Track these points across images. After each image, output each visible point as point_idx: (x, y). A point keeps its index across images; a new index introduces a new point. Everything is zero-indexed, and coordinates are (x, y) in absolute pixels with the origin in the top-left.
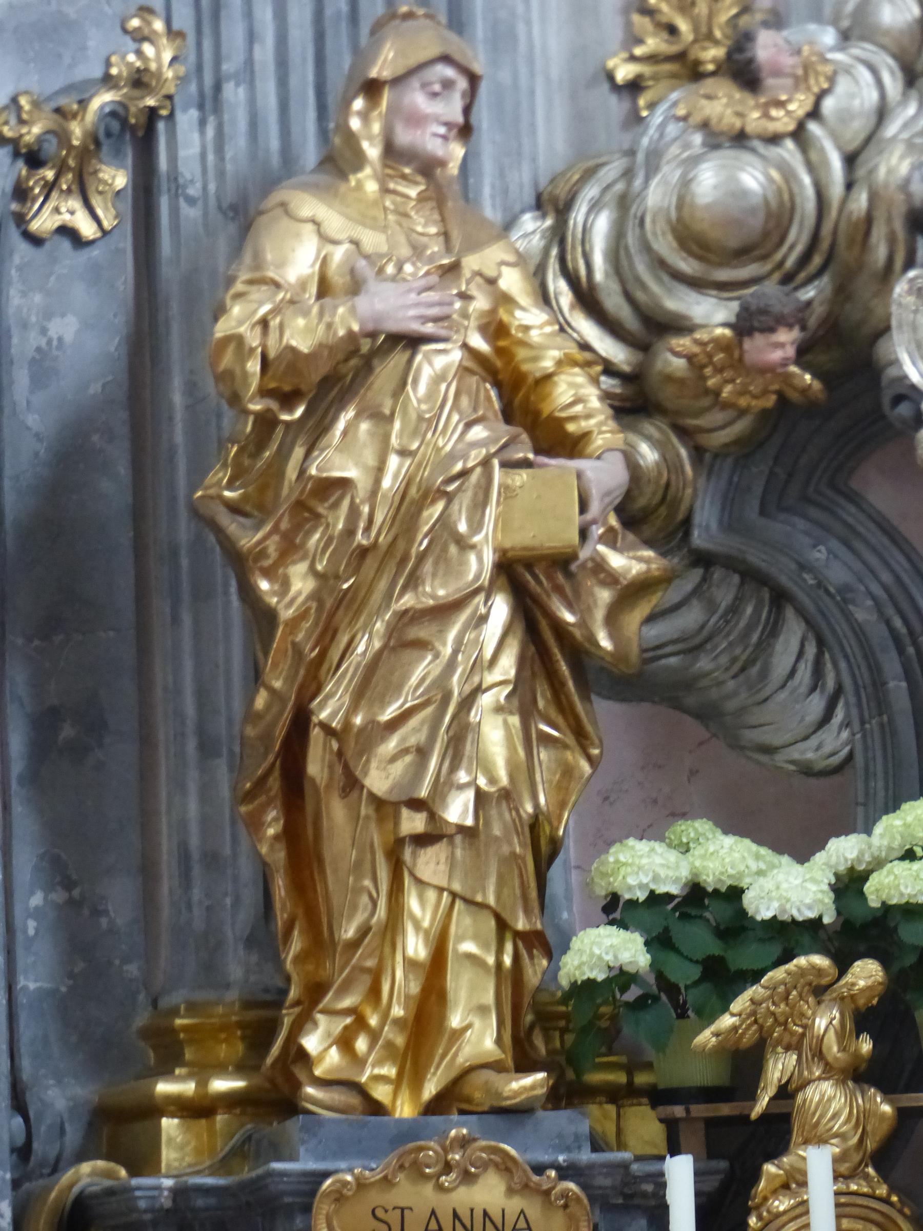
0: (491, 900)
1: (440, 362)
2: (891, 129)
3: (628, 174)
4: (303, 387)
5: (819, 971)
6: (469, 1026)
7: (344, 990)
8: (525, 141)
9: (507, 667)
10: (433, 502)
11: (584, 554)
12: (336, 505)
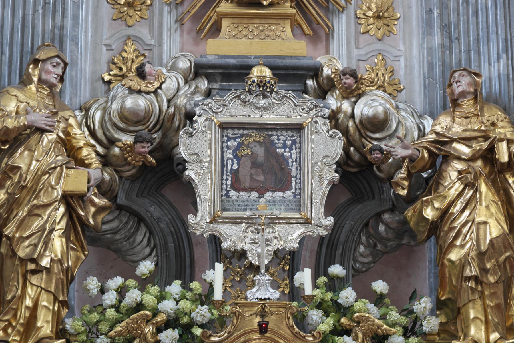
0: (53, 290)
1: (50, 137)
2: (181, 93)
3: (107, 102)
4: (9, 139)
5: (147, 316)
6: (43, 326)
7: (6, 314)
8: (78, 92)
9: (63, 224)
10: (45, 175)
11: (88, 195)
12: (15, 174)
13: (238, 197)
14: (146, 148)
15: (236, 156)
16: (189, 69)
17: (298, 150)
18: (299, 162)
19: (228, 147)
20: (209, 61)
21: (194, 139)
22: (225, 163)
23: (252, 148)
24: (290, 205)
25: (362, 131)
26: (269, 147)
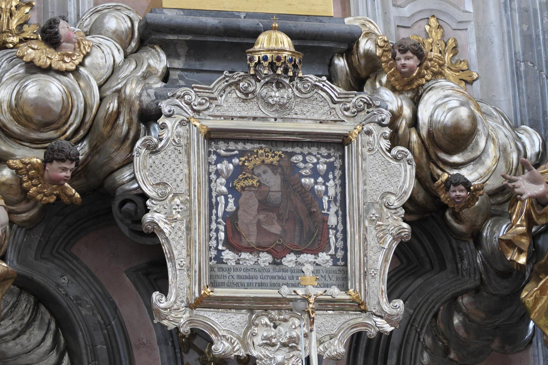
13: (237, 263)
14: (61, 171)
15: (232, 190)
16: (129, 32)
17: (338, 182)
18: (341, 201)
19: (218, 173)
20: (171, 20)
21: (160, 156)
22: (214, 200)
23: (259, 175)
24: (327, 278)
25: (431, 150)
26: (289, 174)
